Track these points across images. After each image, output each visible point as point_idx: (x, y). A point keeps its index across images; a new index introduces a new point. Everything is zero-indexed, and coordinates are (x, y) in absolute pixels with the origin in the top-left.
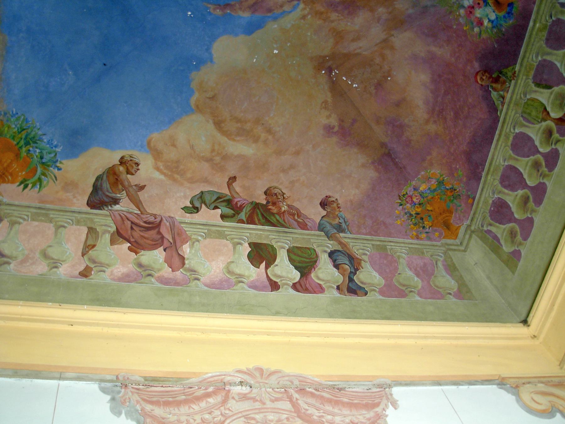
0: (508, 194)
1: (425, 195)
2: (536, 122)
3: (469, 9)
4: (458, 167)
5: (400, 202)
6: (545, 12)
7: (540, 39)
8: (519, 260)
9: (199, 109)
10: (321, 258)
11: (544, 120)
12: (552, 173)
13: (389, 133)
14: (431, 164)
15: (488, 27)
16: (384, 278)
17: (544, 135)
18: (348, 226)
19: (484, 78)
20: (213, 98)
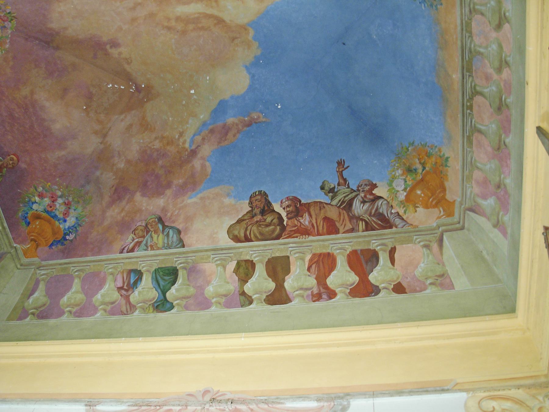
5: (11, 14)
9: (244, 28)
19: (11, 162)
20: (233, 39)
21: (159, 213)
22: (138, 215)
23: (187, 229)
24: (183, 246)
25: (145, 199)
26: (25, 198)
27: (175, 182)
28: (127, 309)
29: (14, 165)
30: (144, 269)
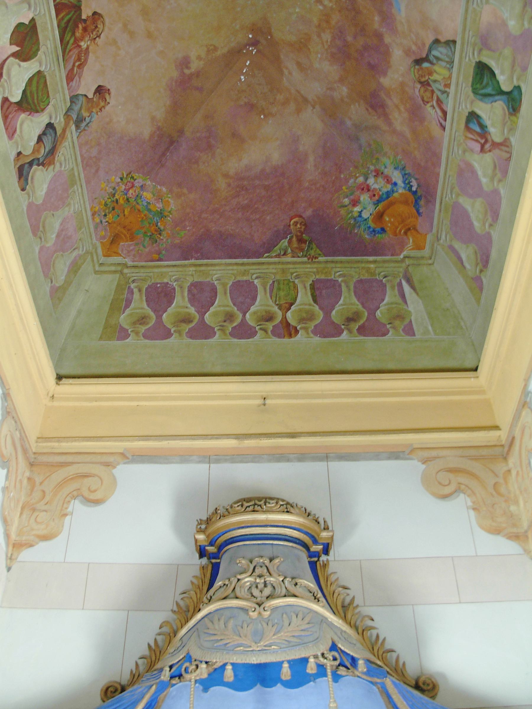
0: (183, 297)
1: (139, 201)
2: (274, 299)
3: (366, 187)
4: (188, 228)
6: (387, 269)
7: (360, 273)
8: (119, 339)
10: (43, 116)
11: (280, 307)
12: (230, 337)
13: (198, 135)
14: (179, 196)
15: (353, 213)
16: (44, 201)
17: (264, 313)
18: (84, 130)
19: (299, 226)
21: (409, 61)
22: (407, 89)
23: (436, 30)
24: (454, 42)
25: (390, 73)
26: (350, 223)
27: (376, 26)
28: (506, 151)
29: (303, 224)
30: (468, 107)
